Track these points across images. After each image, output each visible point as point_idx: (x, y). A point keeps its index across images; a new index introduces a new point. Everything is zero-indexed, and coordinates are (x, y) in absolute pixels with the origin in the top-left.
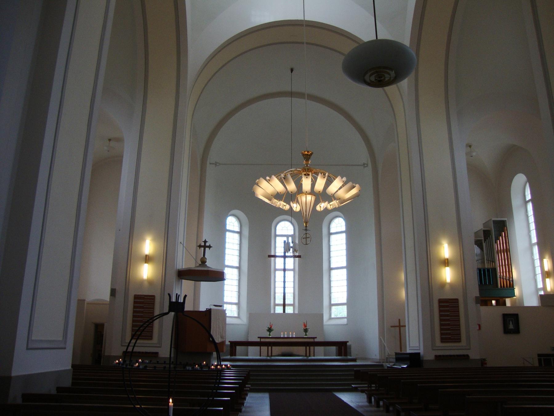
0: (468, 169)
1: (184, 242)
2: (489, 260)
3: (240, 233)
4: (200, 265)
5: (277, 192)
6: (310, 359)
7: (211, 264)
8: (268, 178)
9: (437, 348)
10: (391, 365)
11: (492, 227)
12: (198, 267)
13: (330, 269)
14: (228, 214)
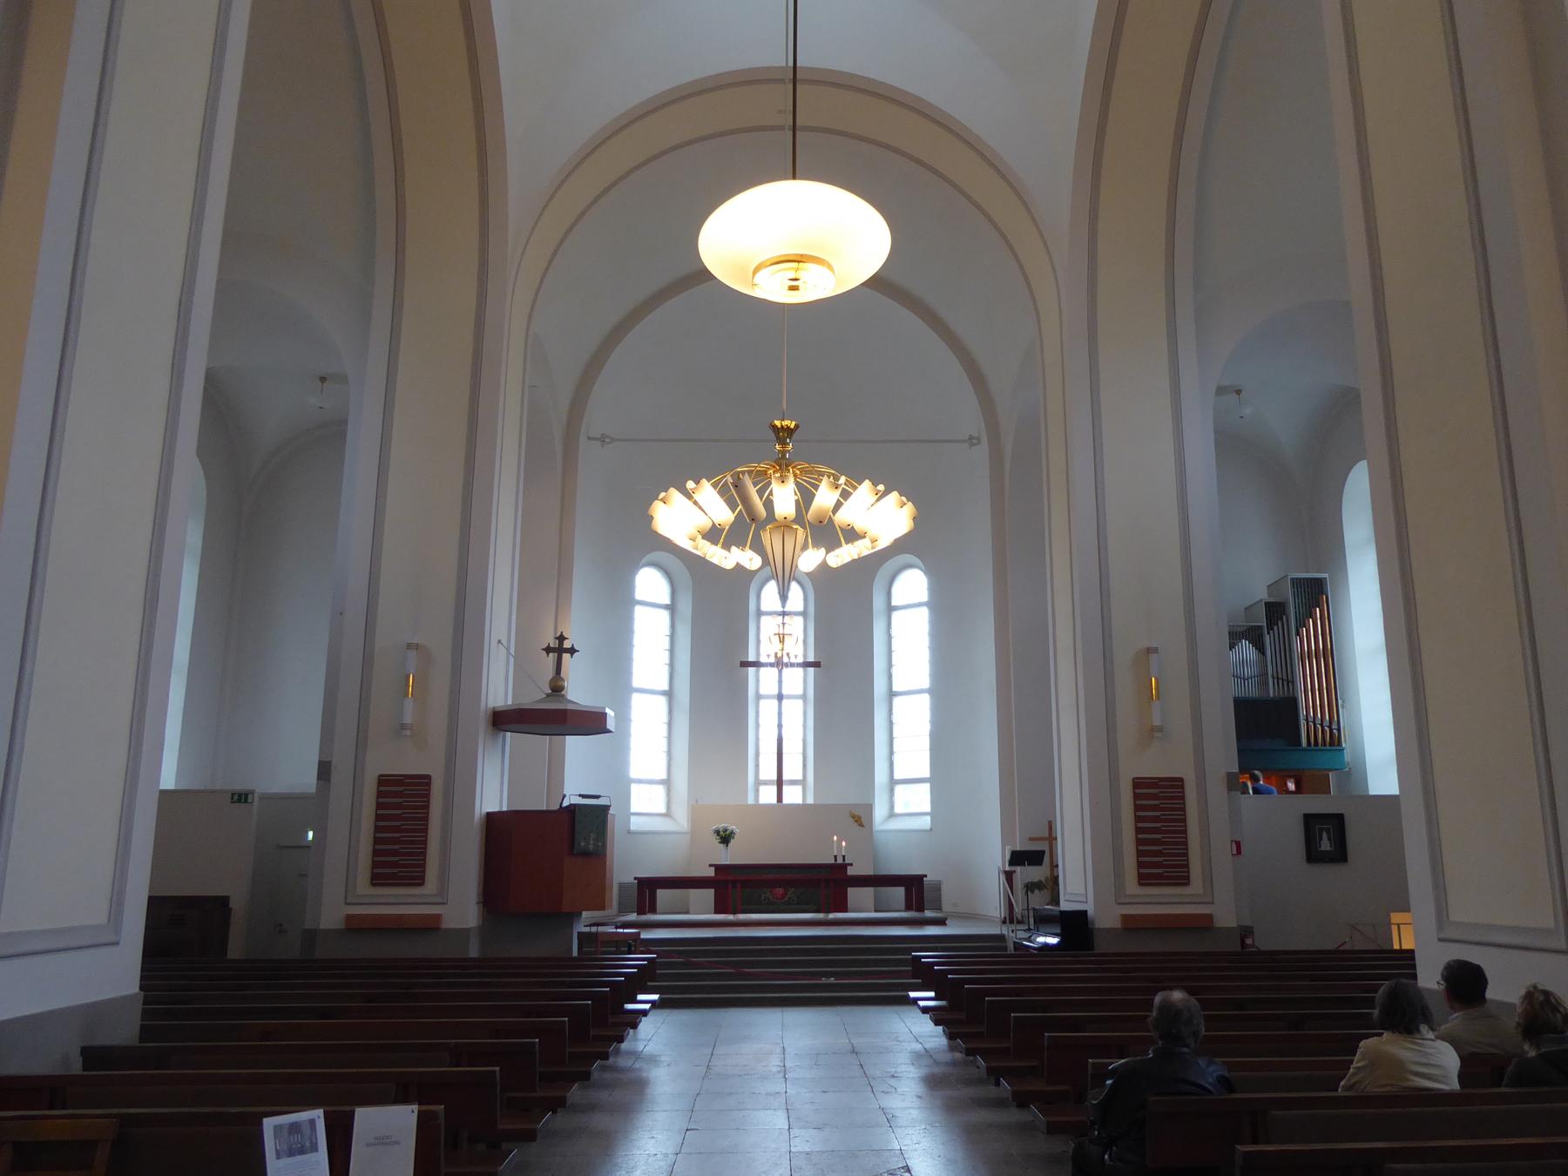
0: (1219, 445)
1: (509, 642)
2: (1280, 676)
3: (672, 608)
4: (548, 695)
5: (711, 524)
6: (832, 919)
7: (580, 692)
8: (690, 485)
9: (1128, 901)
10: (1020, 939)
11: (1288, 595)
12: (541, 701)
13: (892, 694)
14: (641, 559)
